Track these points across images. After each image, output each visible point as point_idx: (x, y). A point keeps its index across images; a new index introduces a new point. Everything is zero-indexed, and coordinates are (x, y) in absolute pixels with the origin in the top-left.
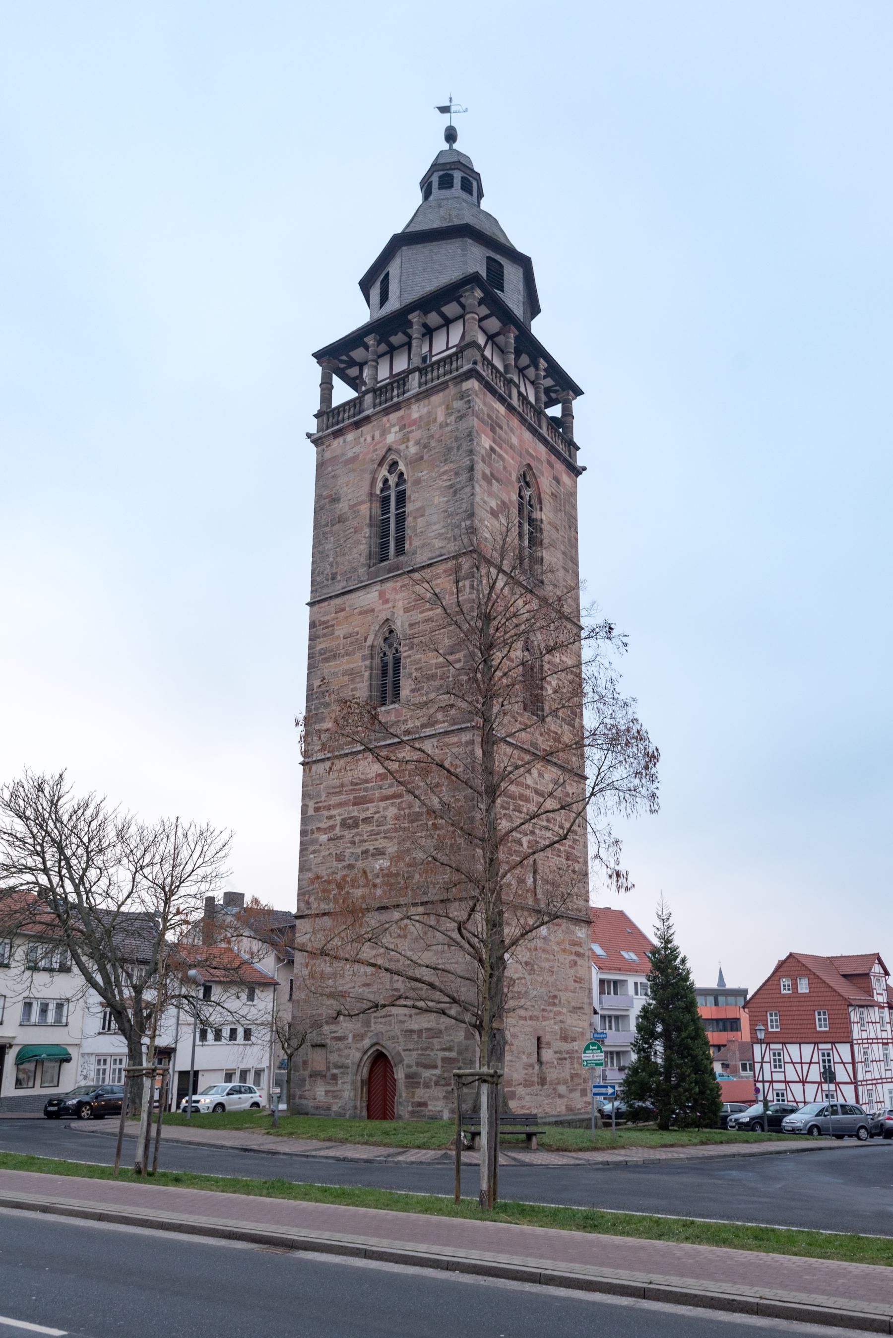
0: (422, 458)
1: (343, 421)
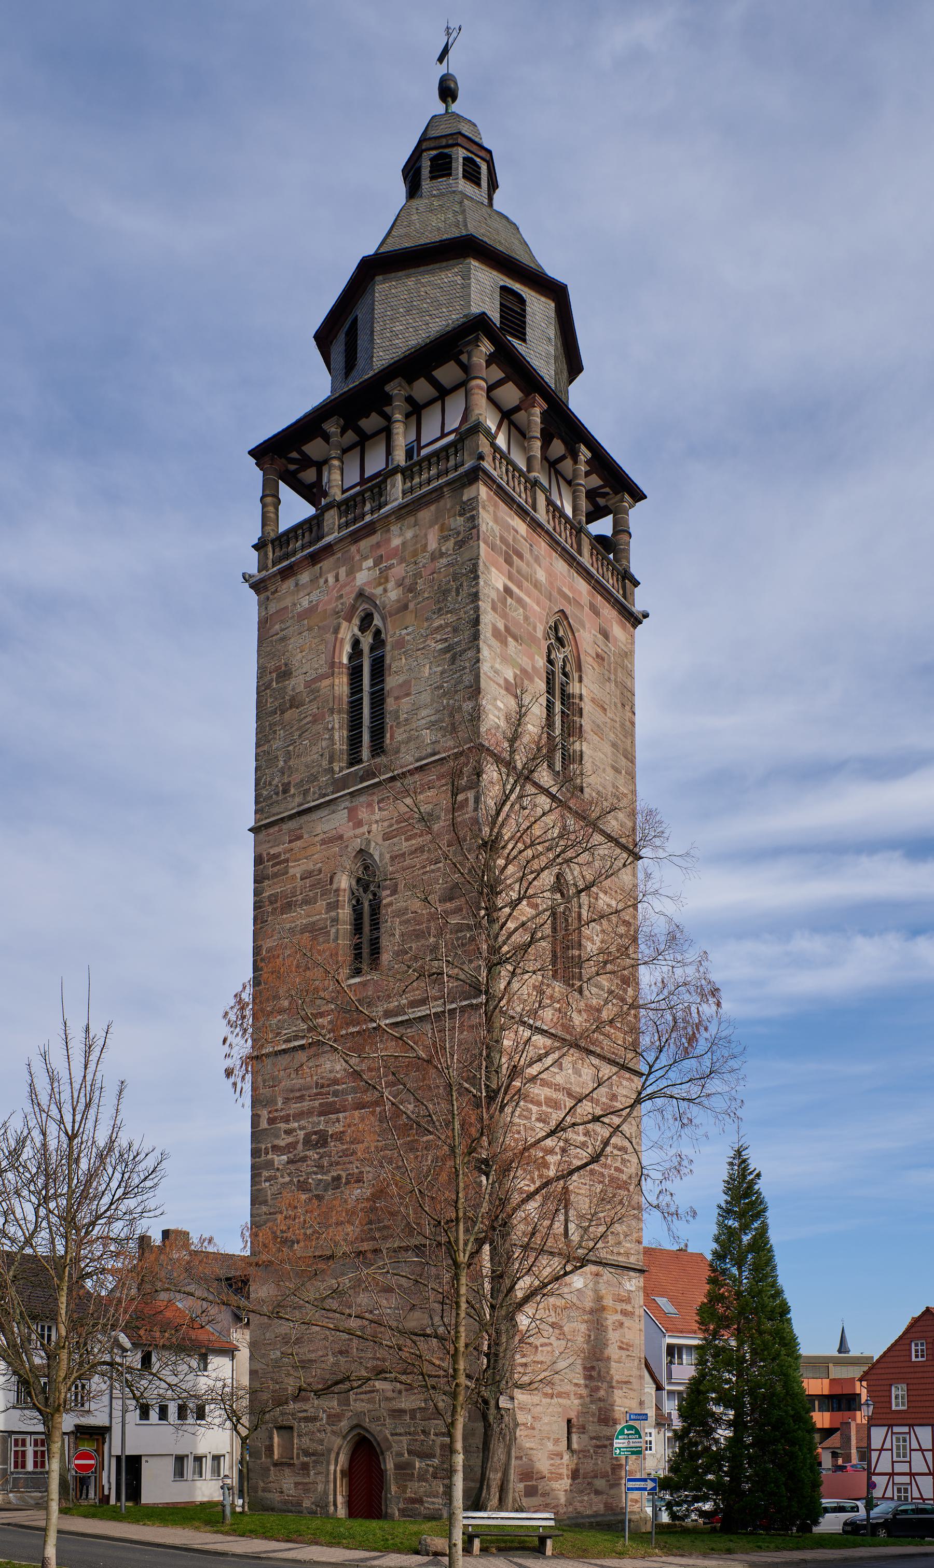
0: (406, 607)
1: (294, 553)
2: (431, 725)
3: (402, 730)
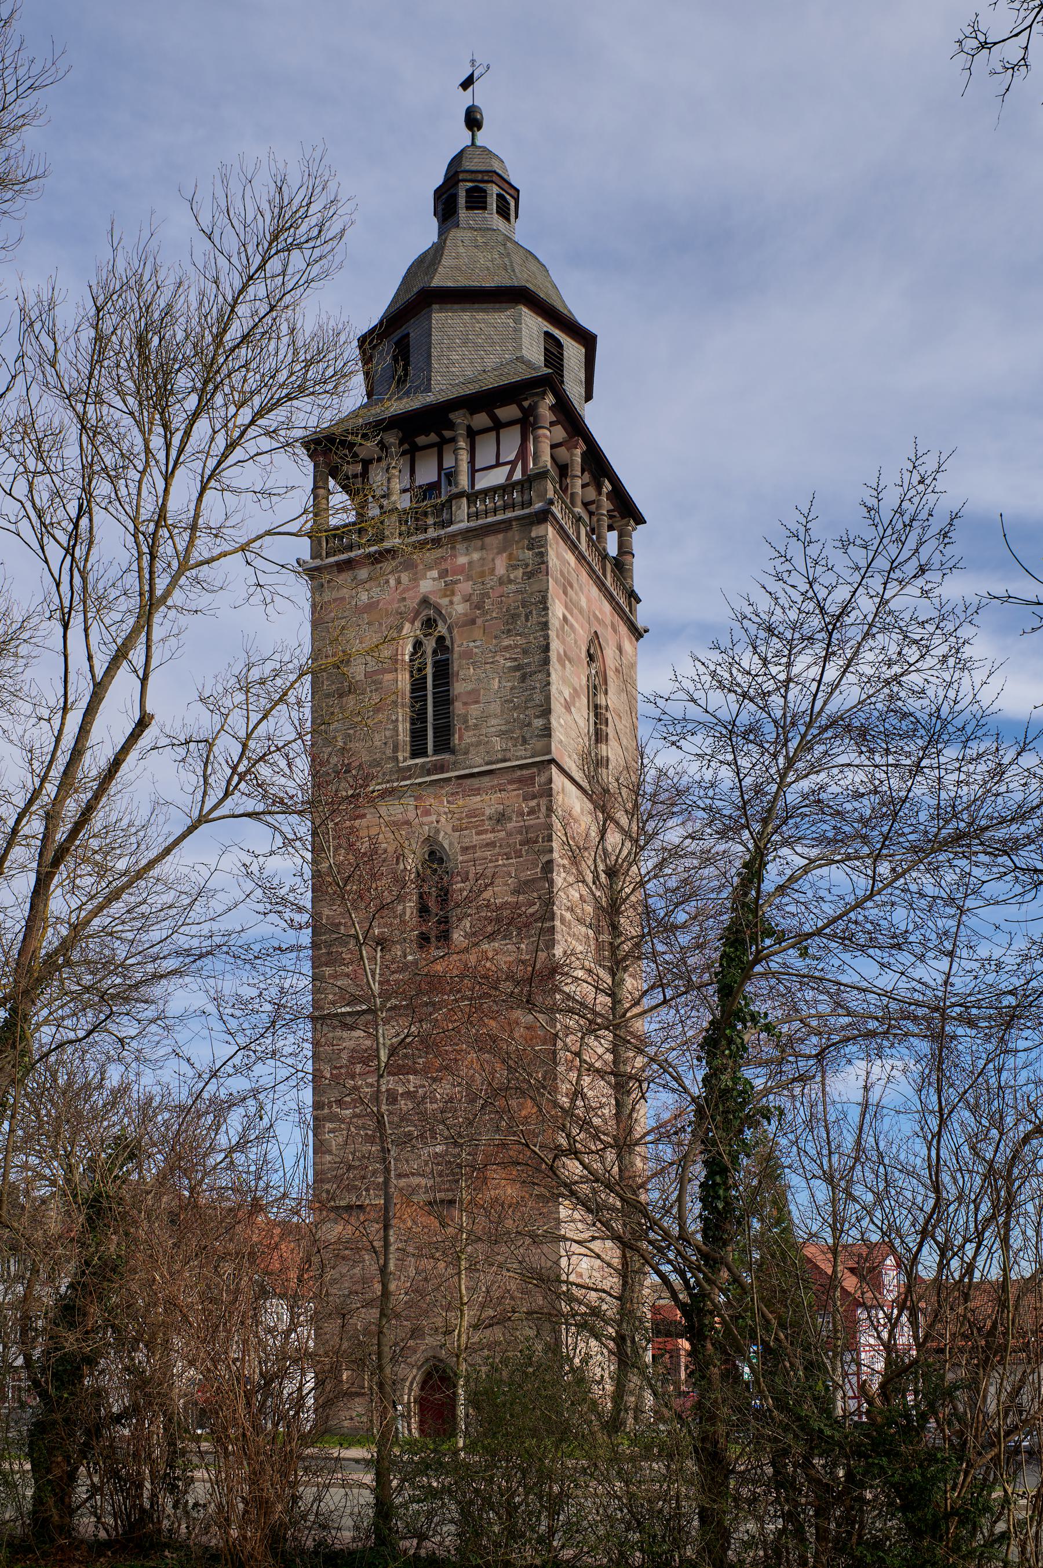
0: (473, 622)
2: (501, 734)
3: (471, 733)
